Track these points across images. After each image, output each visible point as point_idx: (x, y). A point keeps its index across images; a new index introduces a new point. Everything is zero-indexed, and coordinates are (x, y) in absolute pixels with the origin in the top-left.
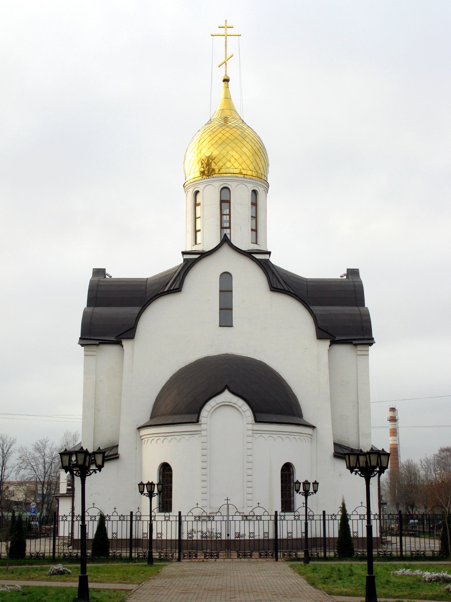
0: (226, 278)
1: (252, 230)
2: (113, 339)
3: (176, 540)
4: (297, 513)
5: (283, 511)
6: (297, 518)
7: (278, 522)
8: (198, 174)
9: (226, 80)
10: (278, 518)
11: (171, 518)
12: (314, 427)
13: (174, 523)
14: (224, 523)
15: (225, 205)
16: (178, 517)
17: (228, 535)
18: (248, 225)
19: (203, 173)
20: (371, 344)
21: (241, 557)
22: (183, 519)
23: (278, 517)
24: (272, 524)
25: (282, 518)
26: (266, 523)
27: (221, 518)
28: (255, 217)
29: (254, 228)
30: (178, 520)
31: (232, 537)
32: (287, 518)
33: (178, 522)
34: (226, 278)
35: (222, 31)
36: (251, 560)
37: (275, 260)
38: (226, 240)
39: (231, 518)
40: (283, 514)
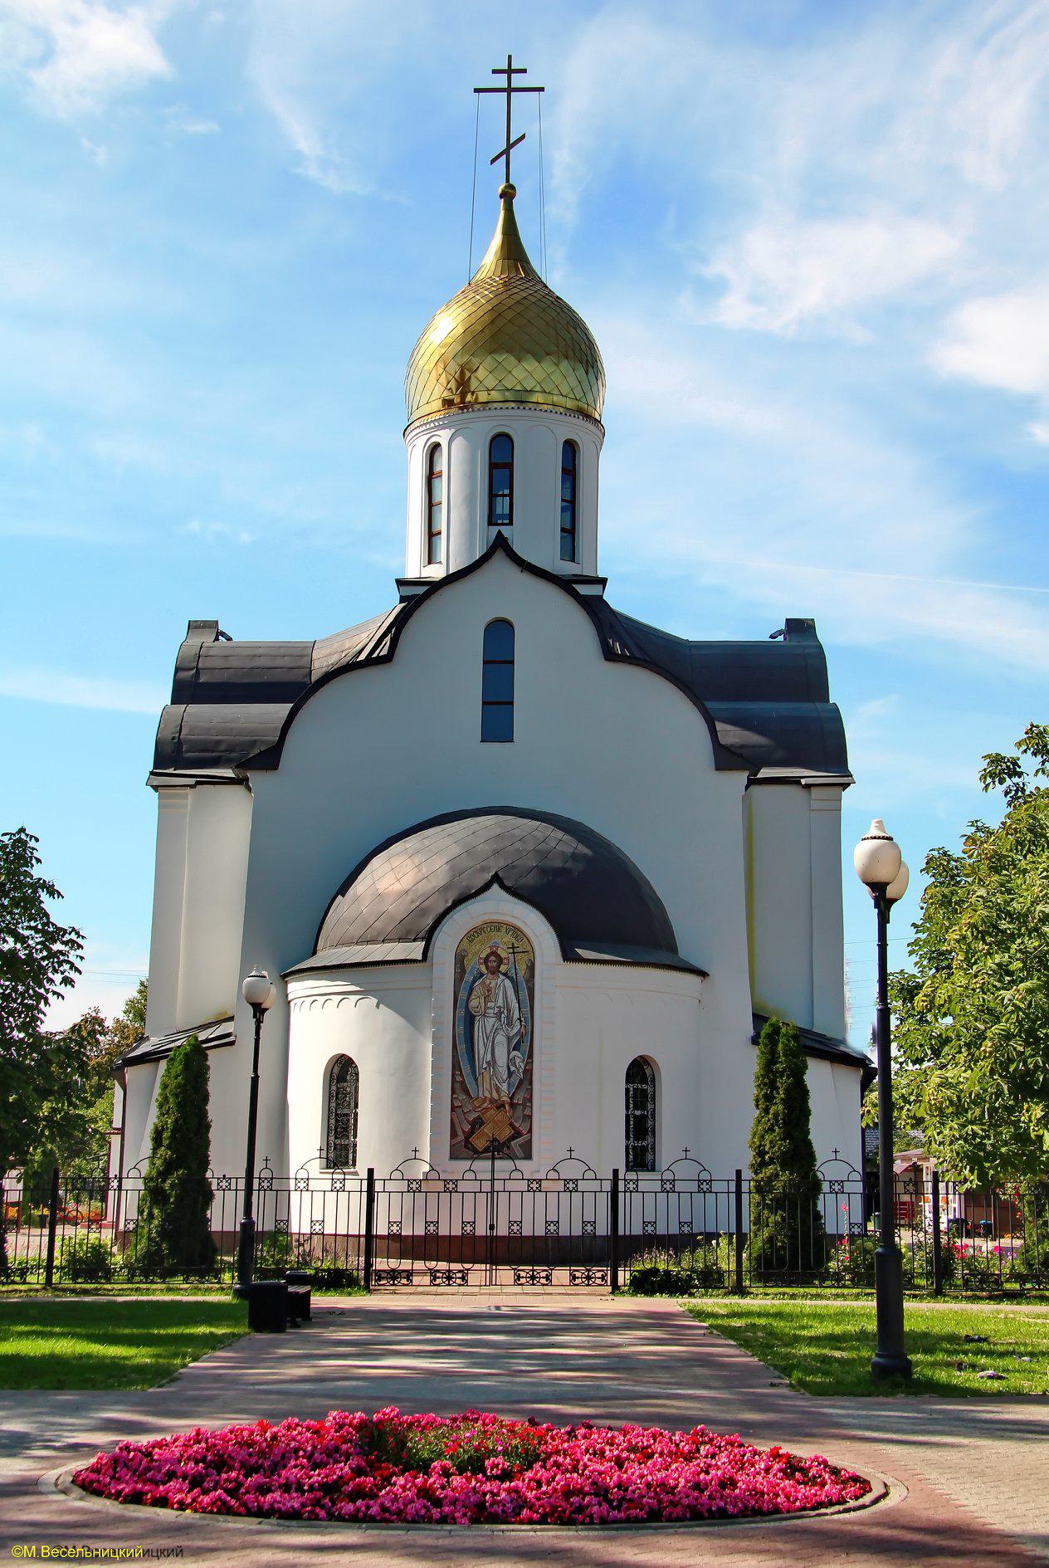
0: (500, 633)
1: (563, 530)
2: (229, 773)
3: (359, 1236)
4: (668, 1176)
5: (628, 1169)
6: (668, 1186)
7: (621, 1195)
8: (437, 405)
9: (508, 194)
10: (621, 1187)
11: (349, 1185)
12: (703, 974)
13: (355, 1197)
14: (482, 1198)
15: (500, 473)
16: (365, 1183)
17: (492, 1227)
18: (554, 519)
19: (448, 403)
20: (845, 786)
21: (523, 1281)
22: (378, 1186)
23: (621, 1185)
24: (604, 1200)
25: (631, 1186)
26: (589, 1197)
27: (475, 1186)
28: (571, 504)
29: (568, 526)
30: (365, 1188)
31: (502, 1230)
32: (642, 1186)
33: (365, 1195)
34: (500, 633)
35: (501, 81)
36: (549, 1289)
37: (616, 598)
38: (500, 545)
39: (487, 1186)
40: (632, 1175)
